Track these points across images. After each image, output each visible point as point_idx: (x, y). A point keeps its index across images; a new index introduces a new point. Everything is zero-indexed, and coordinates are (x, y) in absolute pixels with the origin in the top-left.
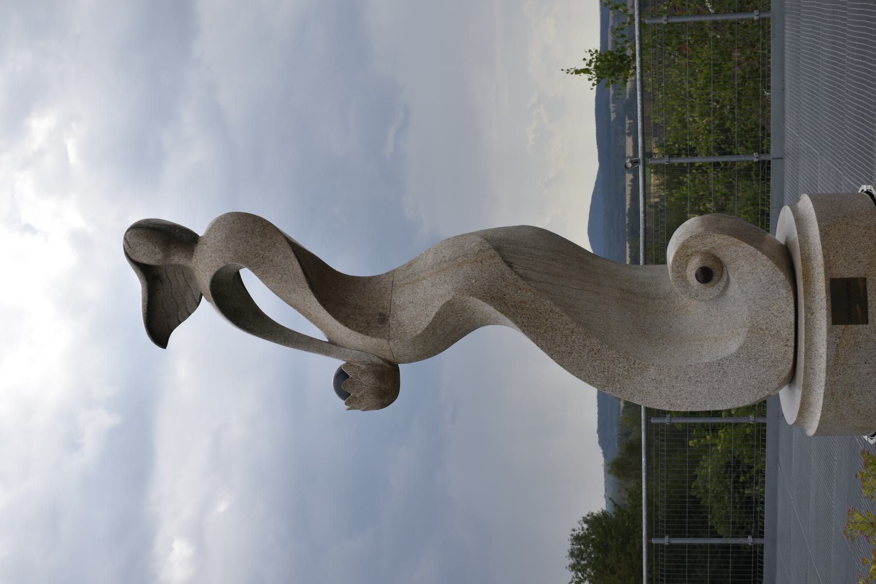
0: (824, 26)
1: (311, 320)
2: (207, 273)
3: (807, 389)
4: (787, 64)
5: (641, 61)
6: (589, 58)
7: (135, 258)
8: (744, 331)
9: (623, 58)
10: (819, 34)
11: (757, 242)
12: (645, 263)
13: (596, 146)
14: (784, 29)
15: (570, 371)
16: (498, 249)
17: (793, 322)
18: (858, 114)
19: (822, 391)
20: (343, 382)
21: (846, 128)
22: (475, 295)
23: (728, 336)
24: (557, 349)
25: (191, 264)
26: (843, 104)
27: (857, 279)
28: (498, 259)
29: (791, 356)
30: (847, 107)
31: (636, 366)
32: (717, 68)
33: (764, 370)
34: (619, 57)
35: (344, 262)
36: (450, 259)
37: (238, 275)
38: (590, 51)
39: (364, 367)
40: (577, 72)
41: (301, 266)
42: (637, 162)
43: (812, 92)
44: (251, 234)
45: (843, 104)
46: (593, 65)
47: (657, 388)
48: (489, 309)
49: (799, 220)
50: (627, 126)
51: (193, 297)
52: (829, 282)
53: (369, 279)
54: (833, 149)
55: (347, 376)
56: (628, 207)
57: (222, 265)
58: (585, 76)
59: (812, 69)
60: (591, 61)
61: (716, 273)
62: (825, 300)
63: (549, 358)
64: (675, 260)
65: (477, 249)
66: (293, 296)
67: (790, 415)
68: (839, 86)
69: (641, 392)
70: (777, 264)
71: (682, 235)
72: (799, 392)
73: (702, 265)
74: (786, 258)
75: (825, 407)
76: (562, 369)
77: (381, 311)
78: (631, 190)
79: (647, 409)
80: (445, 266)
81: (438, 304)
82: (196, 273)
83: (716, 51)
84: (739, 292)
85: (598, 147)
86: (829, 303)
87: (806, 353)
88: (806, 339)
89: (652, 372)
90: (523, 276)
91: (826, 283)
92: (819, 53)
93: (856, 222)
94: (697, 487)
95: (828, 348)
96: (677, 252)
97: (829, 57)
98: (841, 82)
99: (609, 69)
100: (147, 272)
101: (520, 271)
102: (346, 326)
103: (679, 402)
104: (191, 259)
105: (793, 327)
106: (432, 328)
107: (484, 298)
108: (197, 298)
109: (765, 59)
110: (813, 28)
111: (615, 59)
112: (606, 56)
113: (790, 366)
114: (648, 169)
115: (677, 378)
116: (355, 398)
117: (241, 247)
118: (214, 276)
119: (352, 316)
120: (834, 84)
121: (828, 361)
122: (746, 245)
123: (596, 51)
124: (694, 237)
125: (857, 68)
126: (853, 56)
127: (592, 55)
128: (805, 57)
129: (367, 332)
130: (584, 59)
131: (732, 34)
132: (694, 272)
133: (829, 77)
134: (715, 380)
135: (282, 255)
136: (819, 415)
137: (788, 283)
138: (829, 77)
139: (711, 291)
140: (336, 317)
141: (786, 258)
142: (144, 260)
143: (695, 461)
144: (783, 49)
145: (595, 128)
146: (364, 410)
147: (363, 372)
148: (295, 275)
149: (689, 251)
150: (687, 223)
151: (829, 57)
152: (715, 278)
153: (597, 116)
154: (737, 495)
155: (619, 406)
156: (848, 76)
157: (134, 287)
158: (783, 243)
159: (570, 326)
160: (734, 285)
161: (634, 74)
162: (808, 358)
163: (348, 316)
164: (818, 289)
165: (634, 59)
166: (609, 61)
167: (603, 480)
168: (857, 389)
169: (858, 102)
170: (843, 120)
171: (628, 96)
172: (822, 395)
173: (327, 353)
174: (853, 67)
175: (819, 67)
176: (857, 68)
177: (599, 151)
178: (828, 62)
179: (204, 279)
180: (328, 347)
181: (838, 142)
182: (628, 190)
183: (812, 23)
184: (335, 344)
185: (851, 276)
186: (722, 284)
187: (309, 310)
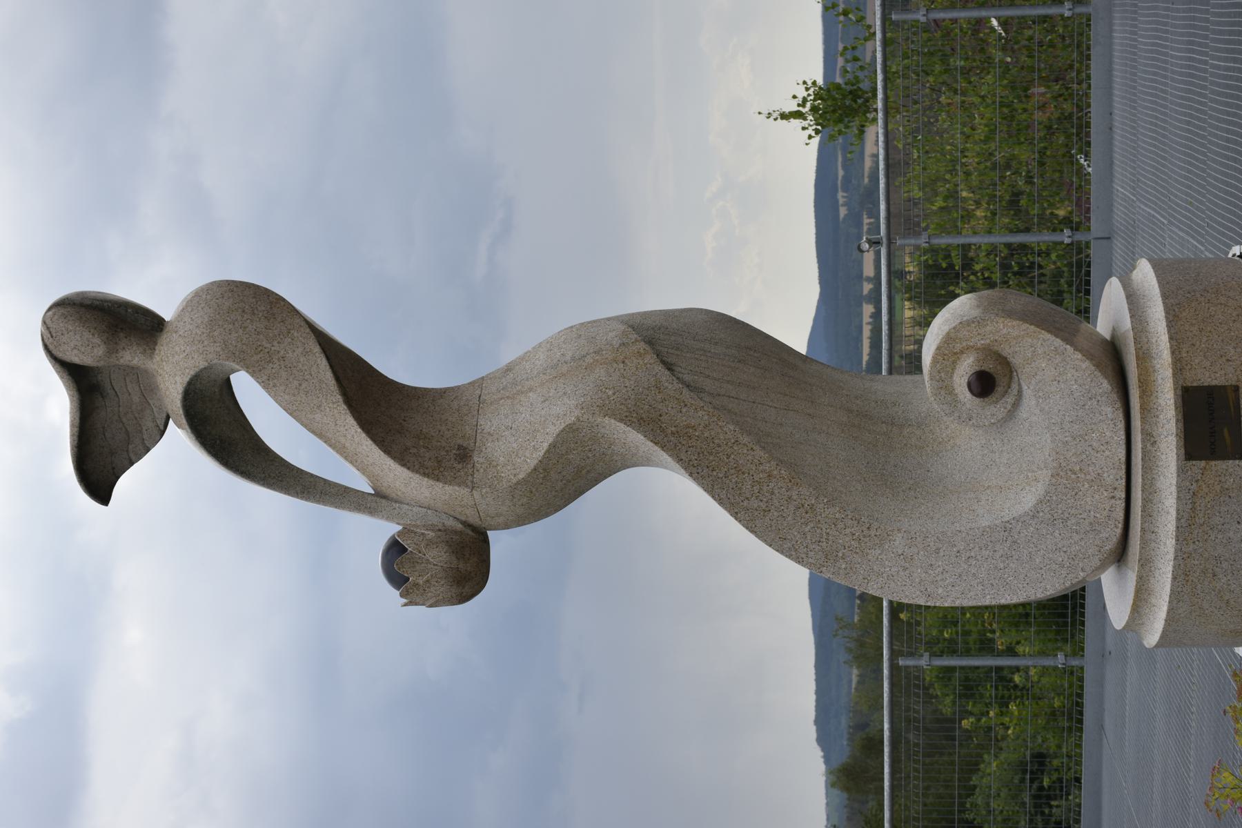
0: (1175, 18)
1: (346, 458)
2: (178, 379)
3: (1146, 564)
4: (1116, 92)
5: (886, 99)
6: (801, 93)
7: (60, 355)
8: (1045, 475)
9: (855, 94)
10: (1167, 32)
11: (1068, 335)
12: (890, 372)
13: (815, 260)
14: (1111, 31)
15: (765, 541)
16: (650, 342)
17: (1123, 459)
18: (1228, 149)
19: (1170, 568)
20: (398, 562)
21: (1209, 175)
22: (613, 415)
23: (1018, 483)
24: (745, 503)
25: (151, 365)
26: (1203, 137)
27: (1224, 387)
28: (650, 358)
29: (1120, 515)
30: (1210, 142)
31: (873, 533)
32: (1005, 110)
33: (1076, 537)
34: (851, 92)
35: (398, 364)
36: (573, 359)
37: (228, 381)
38: (805, 83)
39: (431, 534)
40: (784, 116)
41: (332, 367)
42: (878, 243)
43: (1156, 125)
44: (252, 315)
45: (1203, 137)
46: (808, 105)
47: (905, 569)
48: (635, 439)
49: (1134, 299)
50: (865, 228)
51: (154, 420)
52: (1179, 392)
53: (442, 393)
54: (1189, 211)
55: (404, 550)
56: (865, 358)
57: (203, 364)
58: (796, 123)
59: (1156, 89)
60: (805, 100)
61: (1001, 381)
62: (1173, 422)
63: (732, 519)
64: (935, 361)
65: (616, 343)
66: (318, 416)
67: (1118, 612)
68: (1198, 110)
69: (880, 574)
70: (1097, 366)
71: (947, 320)
72: (1132, 577)
73: (977, 369)
74: (1113, 359)
75: (1175, 596)
76: (752, 537)
77: (460, 442)
78: (872, 331)
79: (891, 602)
80: (565, 368)
81: (554, 430)
82: (159, 379)
83: (1005, 82)
84: (1037, 411)
85: (819, 262)
86: (1181, 425)
87: (1144, 506)
88: (1144, 485)
89: (899, 540)
90: (689, 385)
91: (1175, 394)
92: (1166, 62)
93: (1223, 300)
94: (975, 805)
95: (1178, 498)
96: (938, 348)
97: (1182, 66)
98: (1201, 103)
99: (834, 111)
100: (81, 378)
101: (687, 378)
102: (404, 465)
103: (940, 591)
104: (151, 358)
105: (1124, 467)
106: (543, 469)
107: (626, 420)
108: (161, 423)
109: (1083, 105)
110: (1158, 23)
111: (844, 97)
112: (828, 90)
113: (1119, 531)
114: (898, 298)
115: (937, 551)
116: (416, 585)
117: (234, 335)
118: (189, 383)
119: (414, 451)
120: (1191, 108)
121: (1178, 519)
122: (1048, 336)
123: (814, 83)
124: (965, 324)
125: (1225, 77)
126: (1219, 59)
127: (807, 89)
128: (1145, 72)
129: (441, 477)
130: (794, 97)
131: (1030, 56)
132: (964, 381)
133: (1182, 98)
134: (998, 555)
135: (300, 350)
136: (1165, 608)
137: (1114, 396)
138: (1182, 98)
139: (993, 410)
140: (387, 451)
141: (1113, 359)
142: (76, 359)
143: (972, 766)
144: (1111, 63)
145: (814, 231)
146: (431, 606)
147: (429, 544)
148: (321, 381)
149: (958, 347)
150: (956, 303)
151: (1182, 66)
152: (999, 389)
153: (816, 212)
154: (1039, 818)
155: (850, 681)
156: (1213, 92)
157: (57, 405)
158: (1108, 337)
159: (767, 467)
160: (1029, 401)
161: (875, 120)
162: (1147, 514)
163: (407, 449)
164: (1163, 403)
165: (875, 96)
166: (835, 99)
167: (822, 801)
168: (1225, 565)
169: (1228, 131)
170: (1204, 163)
171: (866, 180)
172: (1170, 575)
173: (371, 511)
174: (1219, 76)
175: (1166, 84)
176: (1225, 77)
177: (819, 268)
178: (1181, 74)
179: (172, 389)
180: (374, 502)
181: (1197, 200)
182: (867, 332)
183: (1156, 15)
184: (385, 497)
185: (1214, 383)
186: (1010, 399)
187: (343, 440)
